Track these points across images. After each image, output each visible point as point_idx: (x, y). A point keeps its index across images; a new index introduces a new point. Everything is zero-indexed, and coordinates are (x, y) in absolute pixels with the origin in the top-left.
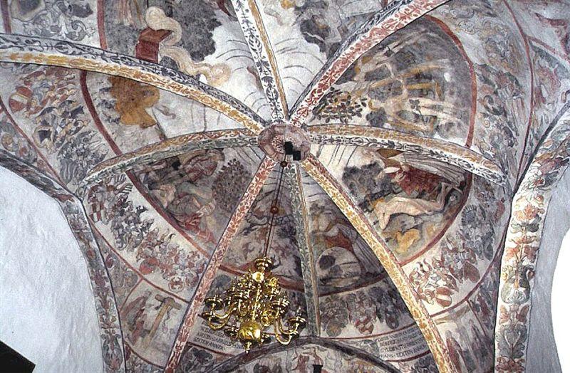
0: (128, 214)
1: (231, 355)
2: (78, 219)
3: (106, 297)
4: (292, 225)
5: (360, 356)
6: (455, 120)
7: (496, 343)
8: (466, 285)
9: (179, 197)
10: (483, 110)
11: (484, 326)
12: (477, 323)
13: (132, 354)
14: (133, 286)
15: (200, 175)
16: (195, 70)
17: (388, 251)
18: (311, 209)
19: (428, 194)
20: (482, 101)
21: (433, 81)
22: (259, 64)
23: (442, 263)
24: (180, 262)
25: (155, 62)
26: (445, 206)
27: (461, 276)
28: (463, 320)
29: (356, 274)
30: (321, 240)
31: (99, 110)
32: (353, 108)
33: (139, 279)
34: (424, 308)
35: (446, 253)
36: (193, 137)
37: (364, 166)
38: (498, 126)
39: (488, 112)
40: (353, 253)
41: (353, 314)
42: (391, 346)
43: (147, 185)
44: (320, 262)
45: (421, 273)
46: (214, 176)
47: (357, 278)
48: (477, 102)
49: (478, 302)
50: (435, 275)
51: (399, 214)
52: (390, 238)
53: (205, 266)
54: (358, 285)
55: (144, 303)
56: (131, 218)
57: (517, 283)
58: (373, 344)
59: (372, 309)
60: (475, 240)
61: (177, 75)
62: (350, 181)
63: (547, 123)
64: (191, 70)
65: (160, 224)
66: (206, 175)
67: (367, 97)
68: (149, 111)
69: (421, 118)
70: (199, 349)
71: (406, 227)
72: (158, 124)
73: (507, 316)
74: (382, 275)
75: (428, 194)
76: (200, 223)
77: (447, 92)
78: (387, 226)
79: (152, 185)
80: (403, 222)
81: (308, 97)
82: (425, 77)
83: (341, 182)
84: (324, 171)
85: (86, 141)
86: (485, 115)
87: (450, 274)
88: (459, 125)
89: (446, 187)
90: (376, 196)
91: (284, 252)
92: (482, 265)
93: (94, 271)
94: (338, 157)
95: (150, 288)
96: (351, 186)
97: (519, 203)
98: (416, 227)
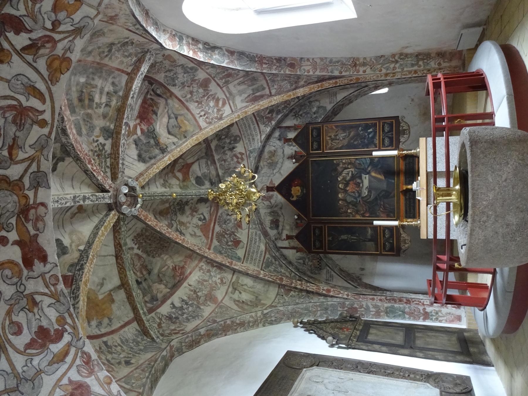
0: (177, 315)
1: (266, 245)
2: (186, 343)
3: (237, 323)
4: (176, 203)
5: (259, 161)
6: (110, 80)
7: (247, 70)
8: (213, 87)
9: (161, 281)
10: (107, 59)
11: (238, 77)
12: (236, 82)
13: (273, 304)
14: (227, 308)
15: (144, 267)
16: (76, 252)
17: (192, 136)
18: (166, 188)
19: (155, 108)
20: (102, 59)
21: (84, 90)
22: (75, 202)
23: (199, 103)
24: (207, 278)
25: (73, 276)
26: (162, 97)
27: (207, 90)
28: (234, 90)
29: (207, 163)
30: (185, 184)
31: (103, 331)
32: (99, 149)
33: (221, 304)
34: (228, 116)
35: (193, 99)
36: (120, 265)
37: (137, 148)
38: (118, 51)
39: (109, 56)
40: (193, 163)
41: (232, 166)
42: (251, 140)
43: (155, 303)
44: (200, 186)
45: (206, 116)
46: (144, 256)
47: (209, 163)
48: (102, 62)
49: (224, 81)
50: (207, 108)
51: (168, 129)
52: (184, 135)
53: (208, 261)
54: (214, 162)
55: (238, 301)
56: (180, 312)
57: (213, 54)
58: (251, 152)
59: (229, 153)
60: (185, 79)
61: (82, 262)
62: (147, 159)
63: (129, 16)
64: (76, 255)
65: (182, 293)
66: (144, 262)
67: (92, 138)
68: (101, 297)
69: (108, 103)
70: (264, 265)
71: (177, 125)
72: (111, 291)
73: (232, 62)
74: (207, 141)
75: (155, 108)
76: (179, 266)
77: (92, 82)
78: (176, 137)
79: (154, 299)
80: (173, 126)
81: (95, 174)
82: (81, 96)
83: (148, 165)
84: (141, 174)
85: (127, 341)
86: (110, 58)
87: (206, 98)
88: (114, 78)
89: (151, 95)
90: (157, 142)
91: (194, 210)
92: (201, 75)
93: (220, 332)
94: (131, 165)
95: (227, 298)
96: (150, 158)
97: (168, 44)
98: (176, 118)
